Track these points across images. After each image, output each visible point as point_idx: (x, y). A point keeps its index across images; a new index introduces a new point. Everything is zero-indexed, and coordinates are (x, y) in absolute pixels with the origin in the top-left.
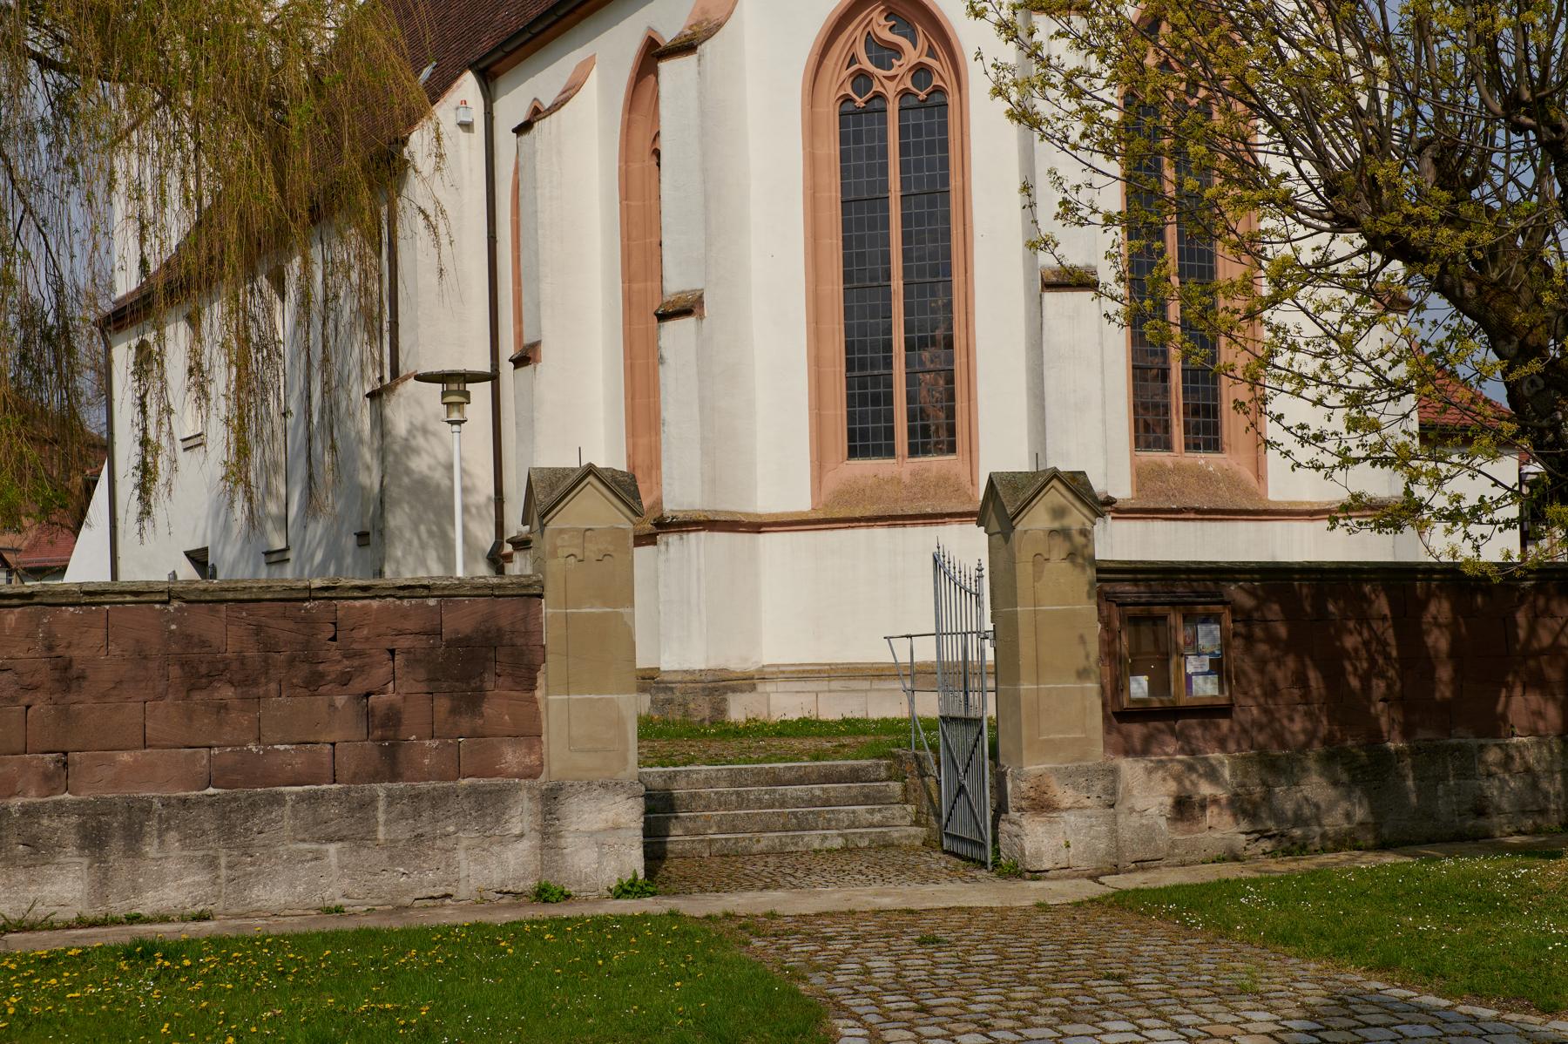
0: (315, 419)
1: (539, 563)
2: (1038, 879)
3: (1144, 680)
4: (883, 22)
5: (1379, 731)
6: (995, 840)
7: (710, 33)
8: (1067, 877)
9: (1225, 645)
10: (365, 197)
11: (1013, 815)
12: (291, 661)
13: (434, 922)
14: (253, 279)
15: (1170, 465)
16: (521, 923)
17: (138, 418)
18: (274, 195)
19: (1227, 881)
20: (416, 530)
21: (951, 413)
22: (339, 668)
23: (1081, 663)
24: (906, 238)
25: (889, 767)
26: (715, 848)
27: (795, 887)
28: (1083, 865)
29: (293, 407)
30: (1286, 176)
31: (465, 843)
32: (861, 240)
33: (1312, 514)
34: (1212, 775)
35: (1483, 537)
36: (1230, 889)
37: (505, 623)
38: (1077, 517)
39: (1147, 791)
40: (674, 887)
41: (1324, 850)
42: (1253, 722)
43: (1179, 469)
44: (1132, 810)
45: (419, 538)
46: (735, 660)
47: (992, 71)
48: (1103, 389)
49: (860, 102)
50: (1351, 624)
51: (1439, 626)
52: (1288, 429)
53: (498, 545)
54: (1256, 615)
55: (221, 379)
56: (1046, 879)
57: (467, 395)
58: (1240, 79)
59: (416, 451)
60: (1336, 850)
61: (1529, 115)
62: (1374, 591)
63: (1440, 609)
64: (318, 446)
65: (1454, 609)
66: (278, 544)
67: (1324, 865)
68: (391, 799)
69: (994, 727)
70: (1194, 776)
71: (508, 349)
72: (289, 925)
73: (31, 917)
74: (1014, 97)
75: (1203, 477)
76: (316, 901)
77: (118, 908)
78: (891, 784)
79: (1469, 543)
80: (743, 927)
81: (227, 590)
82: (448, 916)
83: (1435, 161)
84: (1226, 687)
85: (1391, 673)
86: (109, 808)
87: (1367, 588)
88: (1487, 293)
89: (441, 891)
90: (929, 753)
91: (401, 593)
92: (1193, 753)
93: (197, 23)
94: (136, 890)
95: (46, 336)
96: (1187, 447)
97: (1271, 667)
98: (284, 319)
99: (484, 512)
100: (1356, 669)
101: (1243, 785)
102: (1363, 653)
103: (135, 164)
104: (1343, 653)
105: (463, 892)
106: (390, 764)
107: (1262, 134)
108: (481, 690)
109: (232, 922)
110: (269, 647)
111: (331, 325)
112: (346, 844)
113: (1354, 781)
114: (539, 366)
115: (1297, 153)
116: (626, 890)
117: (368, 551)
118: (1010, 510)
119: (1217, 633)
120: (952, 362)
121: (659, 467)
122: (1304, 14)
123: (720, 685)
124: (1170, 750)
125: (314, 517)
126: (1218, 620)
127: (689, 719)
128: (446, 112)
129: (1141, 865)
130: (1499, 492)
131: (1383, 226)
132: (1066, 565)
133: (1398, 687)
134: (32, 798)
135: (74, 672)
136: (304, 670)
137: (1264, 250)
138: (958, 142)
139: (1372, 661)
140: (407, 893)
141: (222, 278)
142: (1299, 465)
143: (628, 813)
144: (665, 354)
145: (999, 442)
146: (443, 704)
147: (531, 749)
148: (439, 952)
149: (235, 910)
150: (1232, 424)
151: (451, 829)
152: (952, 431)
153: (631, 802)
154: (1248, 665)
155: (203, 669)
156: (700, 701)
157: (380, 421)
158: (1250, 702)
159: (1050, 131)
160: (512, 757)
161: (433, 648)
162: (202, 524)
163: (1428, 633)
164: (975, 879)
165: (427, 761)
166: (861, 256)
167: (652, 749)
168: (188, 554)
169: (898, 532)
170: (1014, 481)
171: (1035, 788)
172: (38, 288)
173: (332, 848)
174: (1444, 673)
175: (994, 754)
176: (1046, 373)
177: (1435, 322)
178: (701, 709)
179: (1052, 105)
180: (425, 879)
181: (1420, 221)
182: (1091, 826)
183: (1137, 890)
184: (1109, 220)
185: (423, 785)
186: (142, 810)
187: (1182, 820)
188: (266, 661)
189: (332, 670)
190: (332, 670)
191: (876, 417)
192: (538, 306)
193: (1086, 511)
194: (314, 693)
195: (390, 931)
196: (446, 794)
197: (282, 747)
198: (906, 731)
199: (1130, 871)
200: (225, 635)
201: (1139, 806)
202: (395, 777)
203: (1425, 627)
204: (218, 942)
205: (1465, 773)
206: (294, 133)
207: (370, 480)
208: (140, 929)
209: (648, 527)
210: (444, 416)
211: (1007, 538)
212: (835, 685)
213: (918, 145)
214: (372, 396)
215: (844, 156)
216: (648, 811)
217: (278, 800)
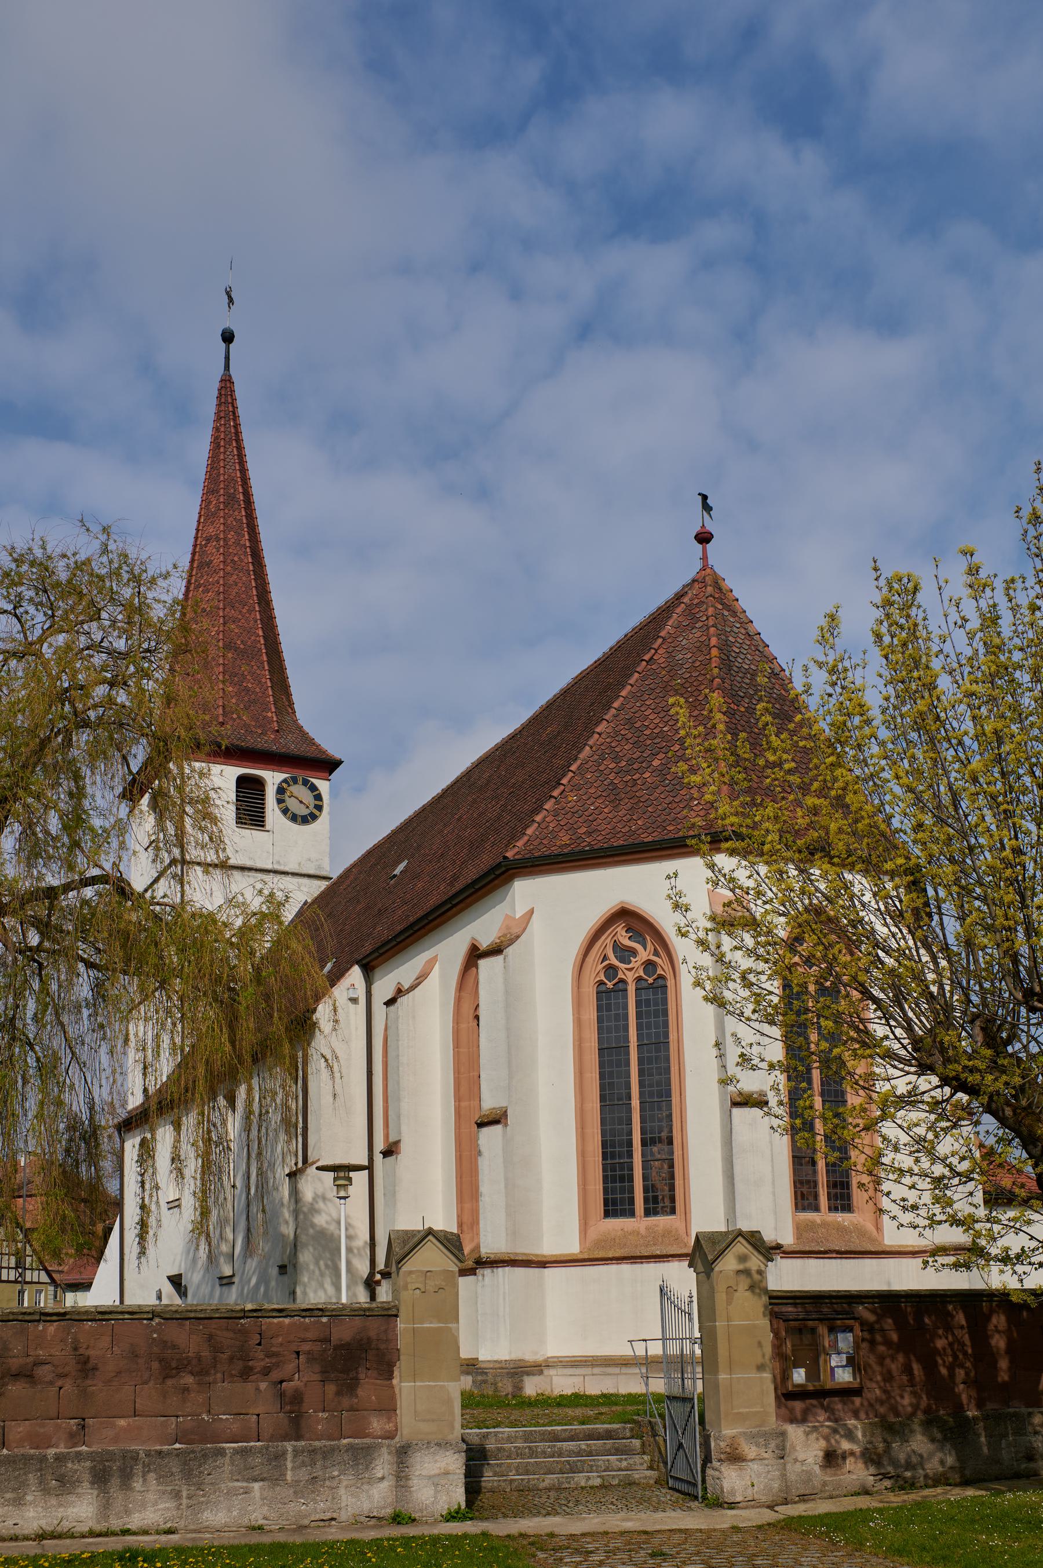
0: (253, 1191)
1: (395, 1292)
2: (733, 1508)
3: (802, 1371)
4: (624, 934)
5: (962, 1405)
6: (704, 1481)
7: (512, 942)
8: (753, 1507)
9: (857, 1346)
10: (286, 1048)
11: (716, 1464)
12: (231, 1359)
13: (323, 1538)
14: (215, 1099)
15: (819, 1222)
16: (381, 1540)
17: (139, 1191)
18: (228, 1047)
19: (861, 1510)
20: (317, 1263)
21: (672, 1188)
22: (262, 1363)
23: (760, 1360)
24: (641, 1073)
25: (632, 1430)
26: (514, 1486)
27: (568, 1514)
28: (764, 1499)
29: (238, 1185)
30: (887, 1037)
31: (345, 1483)
32: (611, 1074)
33: (914, 1254)
34: (850, 1436)
35: (1025, 1273)
36: (863, 1516)
37: (372, 1334)
38: (755, 1262)
39: (806, 1447)
40: (486, 1514)
41: (927, 1486)
42: (877, 1399)
43: (825, 1224)
44: (796, 1460)
45: (319, 1269)
46: (529, 1354)
47: (693, 971)
49: (610, 985)
50: (940, 1332)
51: (998, 1332)
52: (894, 1201)
53: (372, 1274)
54: (877, 1326)
55: (192, 1166)
56: (738, 1508)
57: (350, 1179)
58: (854, 978)
59: (318, 1211)
60: (934, 1486)
61: (1040, 1001)
62: (955, 1309)
63: (999, 1320)
64: (254, 1209)
65: (1008, 1320)
66: (227, 1271)
67: (926, 1497)
68: (296, 1452)
69: (702, 1399)
70: (837, 1437)
71: (379, 1145)
72: (228, 1539)
73: (59, 1529)
74: (708, 988)
75: (841, 1229)
76: (245, 1522)
77: (116, 1524)
78: (633, 1441)
79: (1015, 1277)
80: (532, 1544)
81: (191, 1311)
82: (333, 1534)
83: (982, 1028)
84: (858, 1376)
85: (968, 1364)
86: (110, 1456)
87: (950, 1307)
88: (1018, 1118)
89: (328, 1515)
90: (659, 1420)
91: (304, 1314)
92: (836, 1421)
93: (184, 939)
94: (128, 1512)
95: (83, 1138)
96: (830, 1209)
97: (888, 1361)
98: (233, 1126)
99: (363, 1252)
100: (944, 1362)
101: (871, 1443)
102: (949, 1351)
103: (141, 1028)
104: (936, 1351)
105: (343, 1516)
106: (296, 1429)
107: (871, 1012)
108: (357, 1379)
109: (189, 1536)
110: (216, 1349)
111: (263, 1130)
112: (266, 1483)
113: (945, 1438)
114: (399, 1157)
115: (892, 1023)
116: (453, 1516)
117: (285, 1278)
118: (710, 1257)
119: (851, 1339)
120: (672, 1153)
121: (478, 1223)
122: (894, 935)
123: (519, 1370)
124: (821, 1419)
125: (251, 1256)
126: (850, 1329)
127: (497, 1393)
128: (340, 992)
129: (803, 1498)
130: (1034, 1244)
131: (953, 1069)
132: (748, 1294)
133: (972, 1374)
134: (62, 1449)
135: (90, 1366)
136: (240, 1364)
137: (874, 1085)
138: (674, 1010)
139: (955, 1357)
140: (306, 1517)
141: (193, 1100)
142: (902, 1226)
143: (454, 1463)
144: (482, 1149)
145: (705, 1211)
146: (331, 1389)
147: (389, 1419)
148: (326, 1561)
149: (192, 1527)
150: (858, 1197)
151: (336, 1473)
152: (673, 1199)
153: (456, 1456)
154: (872, 1360)
155: (174, 1364)
156: (505, 1382)
157: (295, 1192)
158: (874, 1385)
159: (732, 1009)
160: (377, 1424)
161: (325, 1350)
162: (179, 1258)
163: (992, 1337)
164: (690, 1508)
165: (320, 1427)
166: (611, 1084)
167: (472, 1416)
168: (169, 1278)
169: (637, 1267)
170: (713, 1238)
171: (730, 1446)
172: (78, 1104)
173: (256, 1486)
174: (1003, 1364)
175: (702, 1422)
176: (734, 1161)
177: (987, 1132)
178: (506, 1387)
179: (735, 992)
180: (317, 1507)
181: (972, 1070)
183: (800, 1517)
184: (772, 1067)
185: (317, 1444)
186: (132, 1458)
187: (830, 1467)
188: (215, 1358)
189: (258, 1365)
190: (258, 1365)
191: (622, 1190)
192: (399, 1117)
193: (761, 1258)
194: (245, 1381)
195: (294, 1544)
196: (333, 1449)
197: (224, 1417)
198: (643, 1403)
199: (795, 1503)
200: (189, 1342)
201: (801, 1456)
202: (298, 1438)
203: (989, 1333)
204: (180, 1551)
205: (1020, 1432)
206: (242, 1008)
207: (288, 1230)
208: (129, 1538)
209: (470, 1263)
210: (335, 1193)
211: (708, 1276)
212: (596, 1370)
213: (648, 1013)
214: (292, 1175)
215: (600, 1020)
216: (469, 1459)
217: (221, 1452)
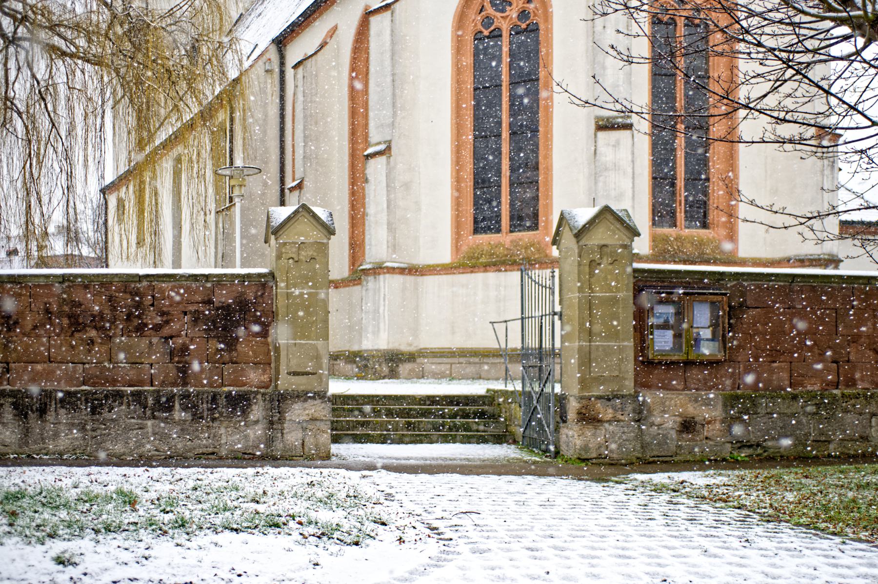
48: (633, 187)
89: (210, 450)
182: (624, 433)
